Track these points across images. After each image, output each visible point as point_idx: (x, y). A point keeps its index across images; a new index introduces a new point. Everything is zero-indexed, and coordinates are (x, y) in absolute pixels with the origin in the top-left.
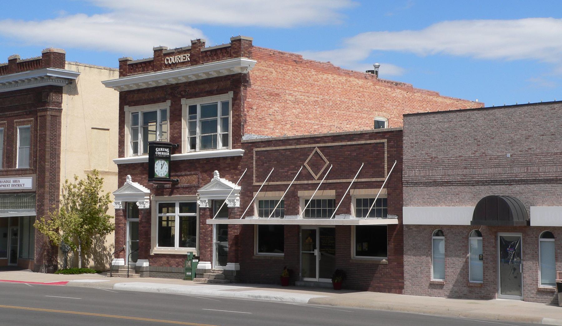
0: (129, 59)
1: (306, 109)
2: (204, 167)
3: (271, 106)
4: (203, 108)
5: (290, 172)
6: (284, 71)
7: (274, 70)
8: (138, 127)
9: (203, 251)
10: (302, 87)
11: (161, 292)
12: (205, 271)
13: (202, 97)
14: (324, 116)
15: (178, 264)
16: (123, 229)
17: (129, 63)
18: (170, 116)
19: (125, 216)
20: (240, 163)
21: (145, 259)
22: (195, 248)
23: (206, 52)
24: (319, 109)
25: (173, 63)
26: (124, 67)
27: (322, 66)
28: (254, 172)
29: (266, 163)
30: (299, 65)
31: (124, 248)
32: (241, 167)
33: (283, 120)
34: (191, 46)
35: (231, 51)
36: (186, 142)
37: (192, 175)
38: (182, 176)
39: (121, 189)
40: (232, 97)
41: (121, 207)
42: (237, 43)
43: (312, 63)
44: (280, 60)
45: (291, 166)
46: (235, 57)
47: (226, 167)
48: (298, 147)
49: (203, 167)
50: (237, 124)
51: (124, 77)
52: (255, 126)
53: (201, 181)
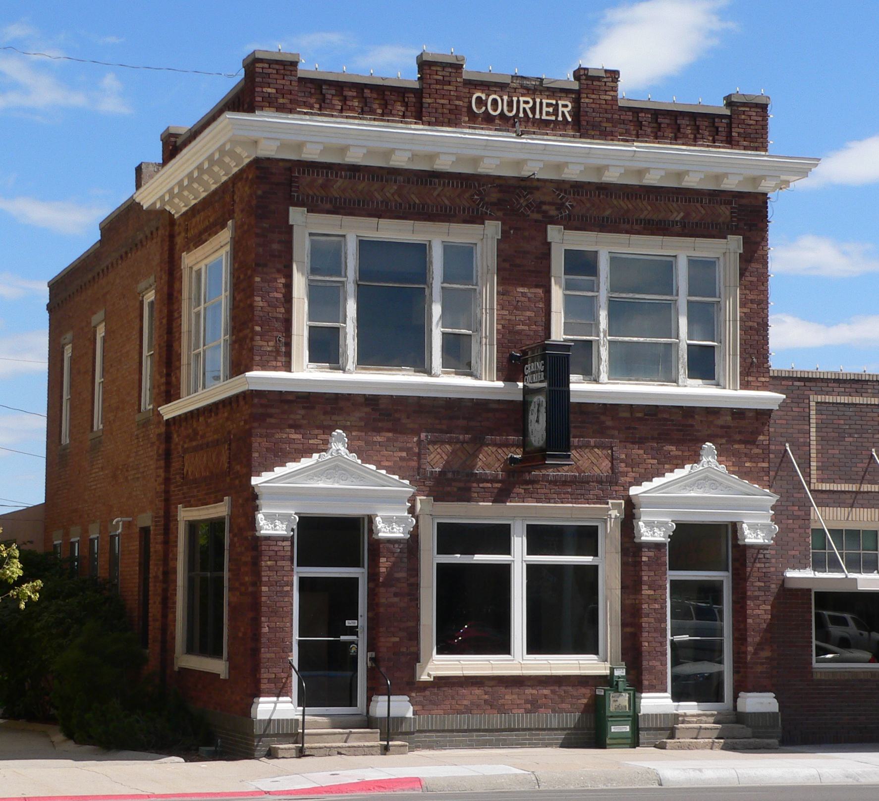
15: (534, 706)
25: (502, 113)
49: (629, 428)
50: (755, 324)
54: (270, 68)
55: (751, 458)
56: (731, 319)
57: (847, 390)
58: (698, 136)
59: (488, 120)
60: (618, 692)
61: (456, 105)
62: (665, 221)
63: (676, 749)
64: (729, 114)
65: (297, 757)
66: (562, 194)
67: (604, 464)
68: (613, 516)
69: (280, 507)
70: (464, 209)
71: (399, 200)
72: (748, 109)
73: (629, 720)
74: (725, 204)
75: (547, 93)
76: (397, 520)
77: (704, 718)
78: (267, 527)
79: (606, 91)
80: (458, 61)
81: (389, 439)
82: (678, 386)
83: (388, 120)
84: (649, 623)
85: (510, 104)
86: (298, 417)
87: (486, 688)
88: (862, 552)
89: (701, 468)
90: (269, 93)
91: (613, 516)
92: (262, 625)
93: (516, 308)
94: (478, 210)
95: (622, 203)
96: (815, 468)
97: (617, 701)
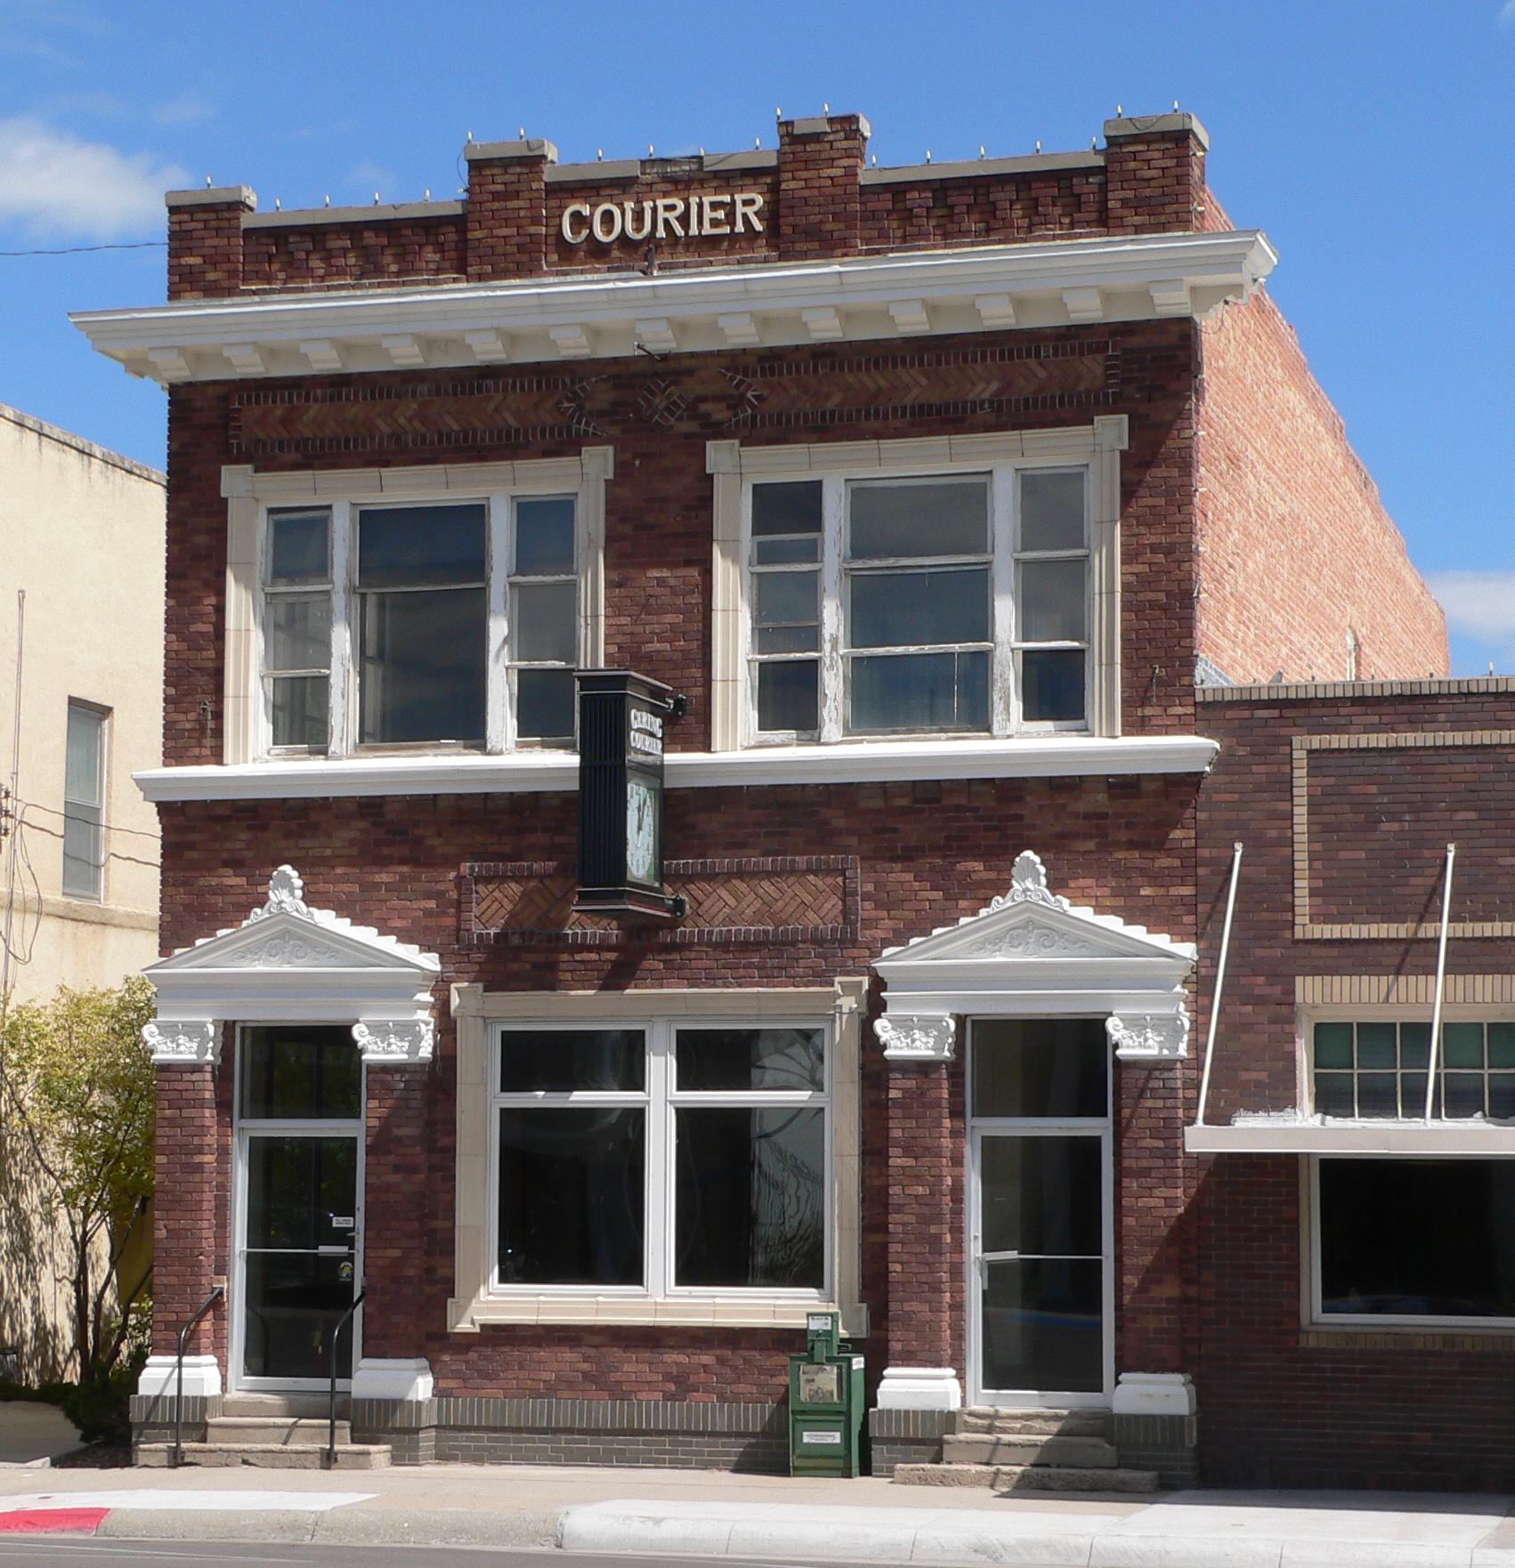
15: (682, 1385)
17: (246, 221)
22: (812, 1292)
28: (1302, 862)
29: (1395, 817)
32: (1192, 833)
37: (793, 872)
38: (711, 877)
42: (1157, 155)
46: (1139, 229)
47: (1074, 836)
50: (1162, 597)
53: (866, 909)
54: (192, 220)
55: (1154, 878)
56: (1104, 590)
57: (1385, 719)
58: (1036, 219)
59: (597, 252)
60: (813, 1363)
61: (530, 235)
62: (956, 405)
63: (914, 1484)
64: (1103, 164)
65: (170, 1467)
67: (828, 906)
68: (845, 1010)
69: (187, 1011)
70: (543, 431)
72: (1140, 148)
73: (840, 1421)
74: (1091, 351)
75: (714, 184)
76: (921, 1023)
77: (1037, 1424)
78: (898, 1043)
79: (833, 160)
80: (531, 150)
81: (403, 877)
82: (993, 738)
83: (403, 282)
84: (903, 1224)
85: (639, 216)
87: (585, 1350)
88: (1486, 1072)
89: (1010, 904)
90: (190, 266)
91: (845, 1010)
92: (156, 1226)
93: (646, 608)
94: (569, 429)
95: (865, 379)
96: (1306, 892)
97: (813, 1380)
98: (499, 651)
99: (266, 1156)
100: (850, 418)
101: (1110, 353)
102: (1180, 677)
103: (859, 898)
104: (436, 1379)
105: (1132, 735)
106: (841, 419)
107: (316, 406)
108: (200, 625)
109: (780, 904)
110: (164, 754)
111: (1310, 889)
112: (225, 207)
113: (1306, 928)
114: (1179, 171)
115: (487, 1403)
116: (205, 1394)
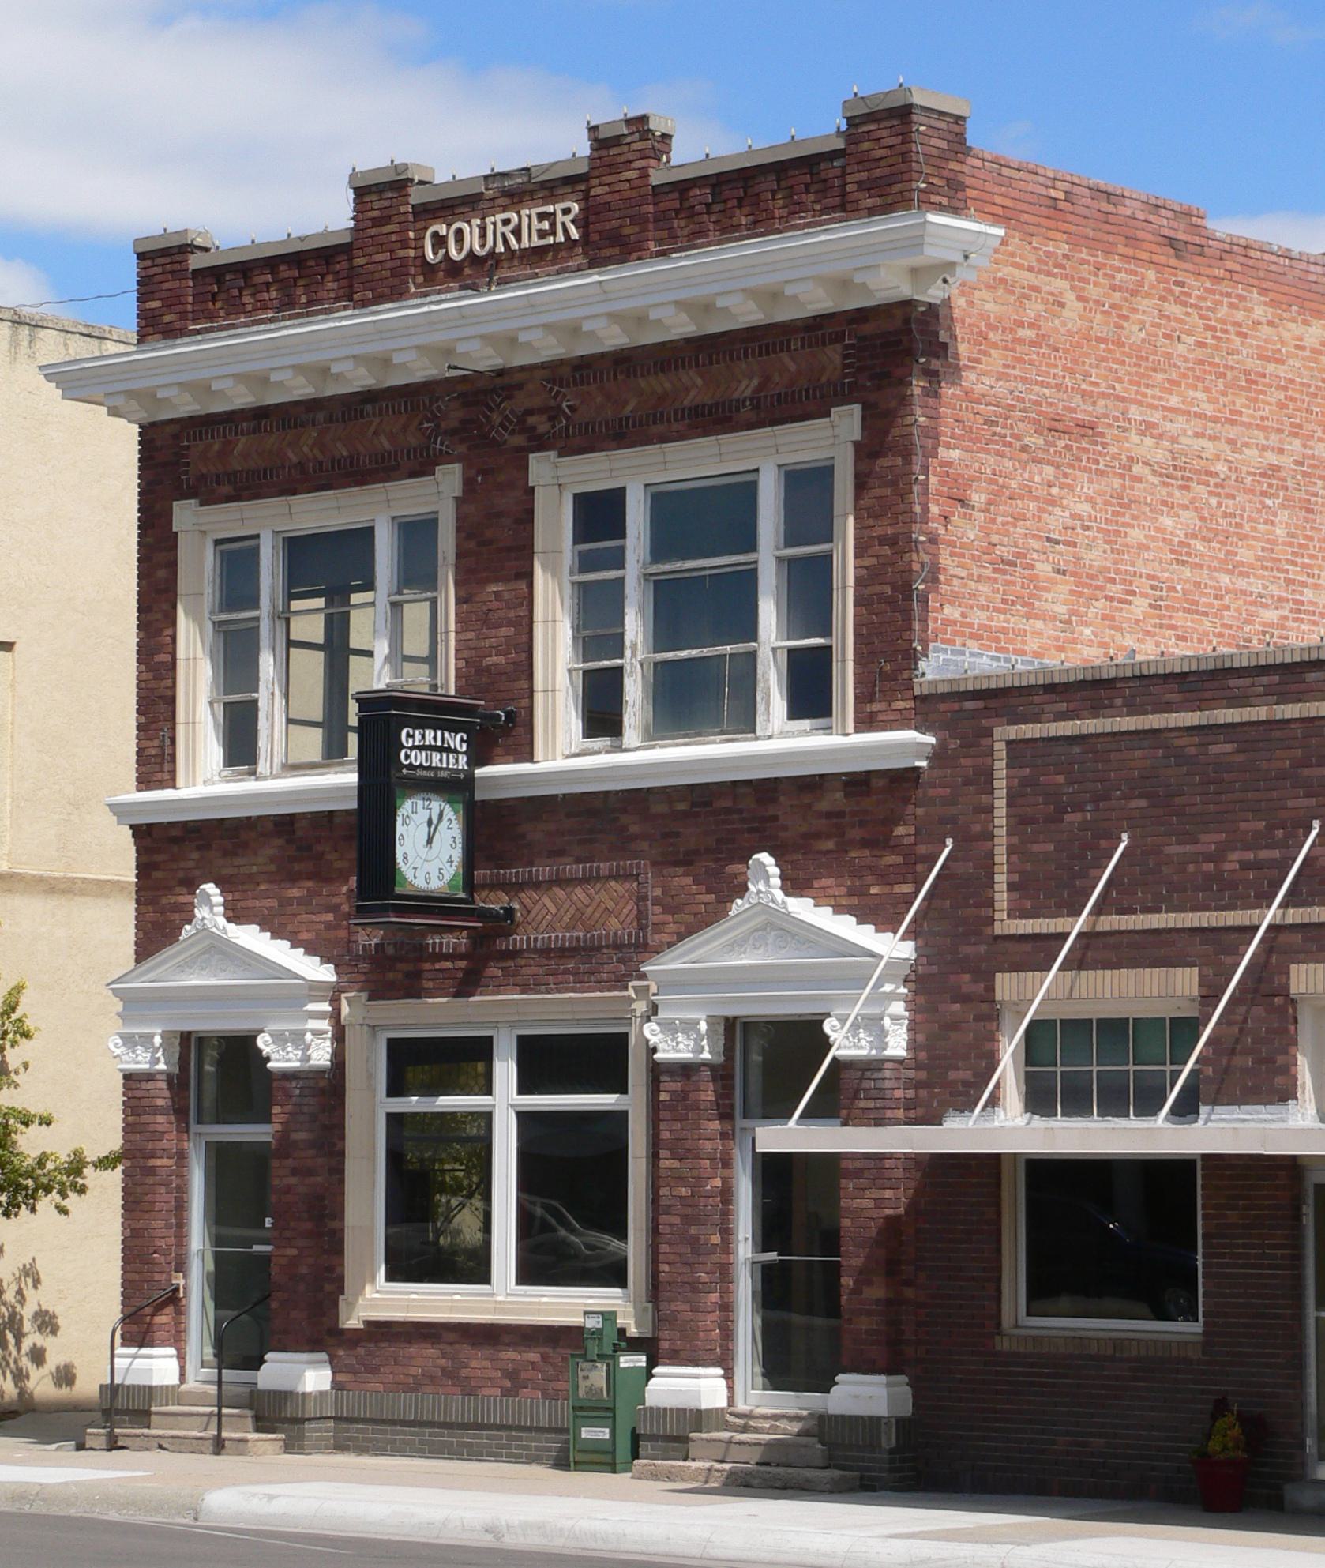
0: (199, 241)
1: (1225, 515)
2: (678, 835)
3: (1055, 491)
4: (662, 502)
5: (1235, 856)
6: (1117, 294)
7: (1073, 288)
8: (257, 619)
9: (678, 1306)
10: (1207, 390)
11: (510, 1541)
12: (699, 1418)
13: (663, 439)
14: (1312, 557)
15: (515, 1382)
16: (167, 1184)
17: (195, 262)
18: (460, 555)
19: (180, 1112)
20: (910, 808)
21: (312, 1351)
22: (617, 1291)
23: (675, 186)
24: (1284, 515)
25: (471, 254)
26: (166, 286)
27: (1297, 273)
28: (1001, 857)
29: (1079, 807)
30: (1190, 267)
31: (177, 1290)
32: (912, 830)
33: (1117, 572)
34: (591, 159)
35: (844, 175)
36: (561, 697)
37: (598, 878)
38: (536, 885)
39: (161, 963)
40: (458, 493)
41: (157, 1061)
43: (1252, 253)
44: (1099, 235)
45: (1243, 826)
46: (872, 212)
47: (818, 835)
48: (1289, 711)
49: (667, 835)
50: (888, 589)
51: (170, 342)
52: (982, 601)
53: (655, 914)
59: (453, 270)
66: (556, 388)
67: (626, 911)
71: (320, 457)
72: (872, 127)
78: (666, 1047)
79: (631, 162)
82: (757, 739)
86: (191, 864)
98: (382, 668)
99: (222, 1158)
100: (641, 425)
101: (847, 342)
102: (901, 670)
103: (649, 903)
104: (334, 1373)
105: (863, 732)
106: (634, 426)
107: (243, 439)
108: (162, 655)
109: (590, 910)
110: (138, 779)
111: (1008, 884)
112: (176, 250)
113: (1007, 925)
114: (904, 148)
115: (371, 1395)
116: (154, 1383)
